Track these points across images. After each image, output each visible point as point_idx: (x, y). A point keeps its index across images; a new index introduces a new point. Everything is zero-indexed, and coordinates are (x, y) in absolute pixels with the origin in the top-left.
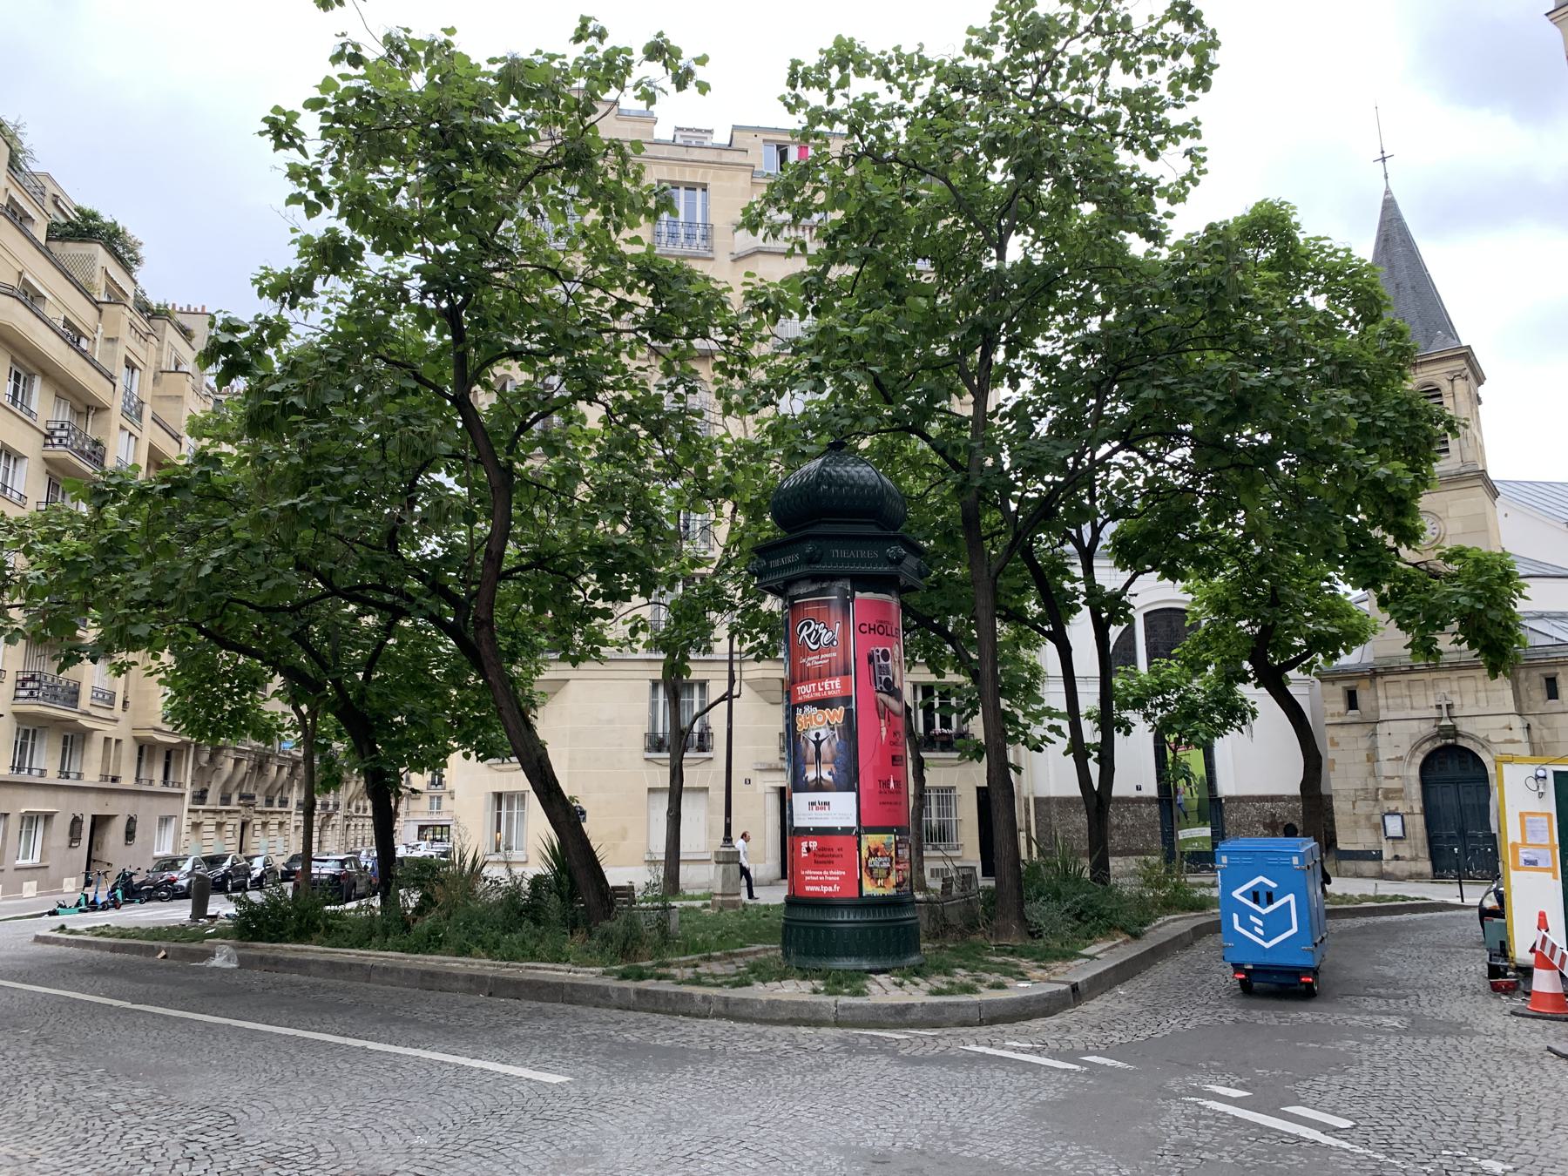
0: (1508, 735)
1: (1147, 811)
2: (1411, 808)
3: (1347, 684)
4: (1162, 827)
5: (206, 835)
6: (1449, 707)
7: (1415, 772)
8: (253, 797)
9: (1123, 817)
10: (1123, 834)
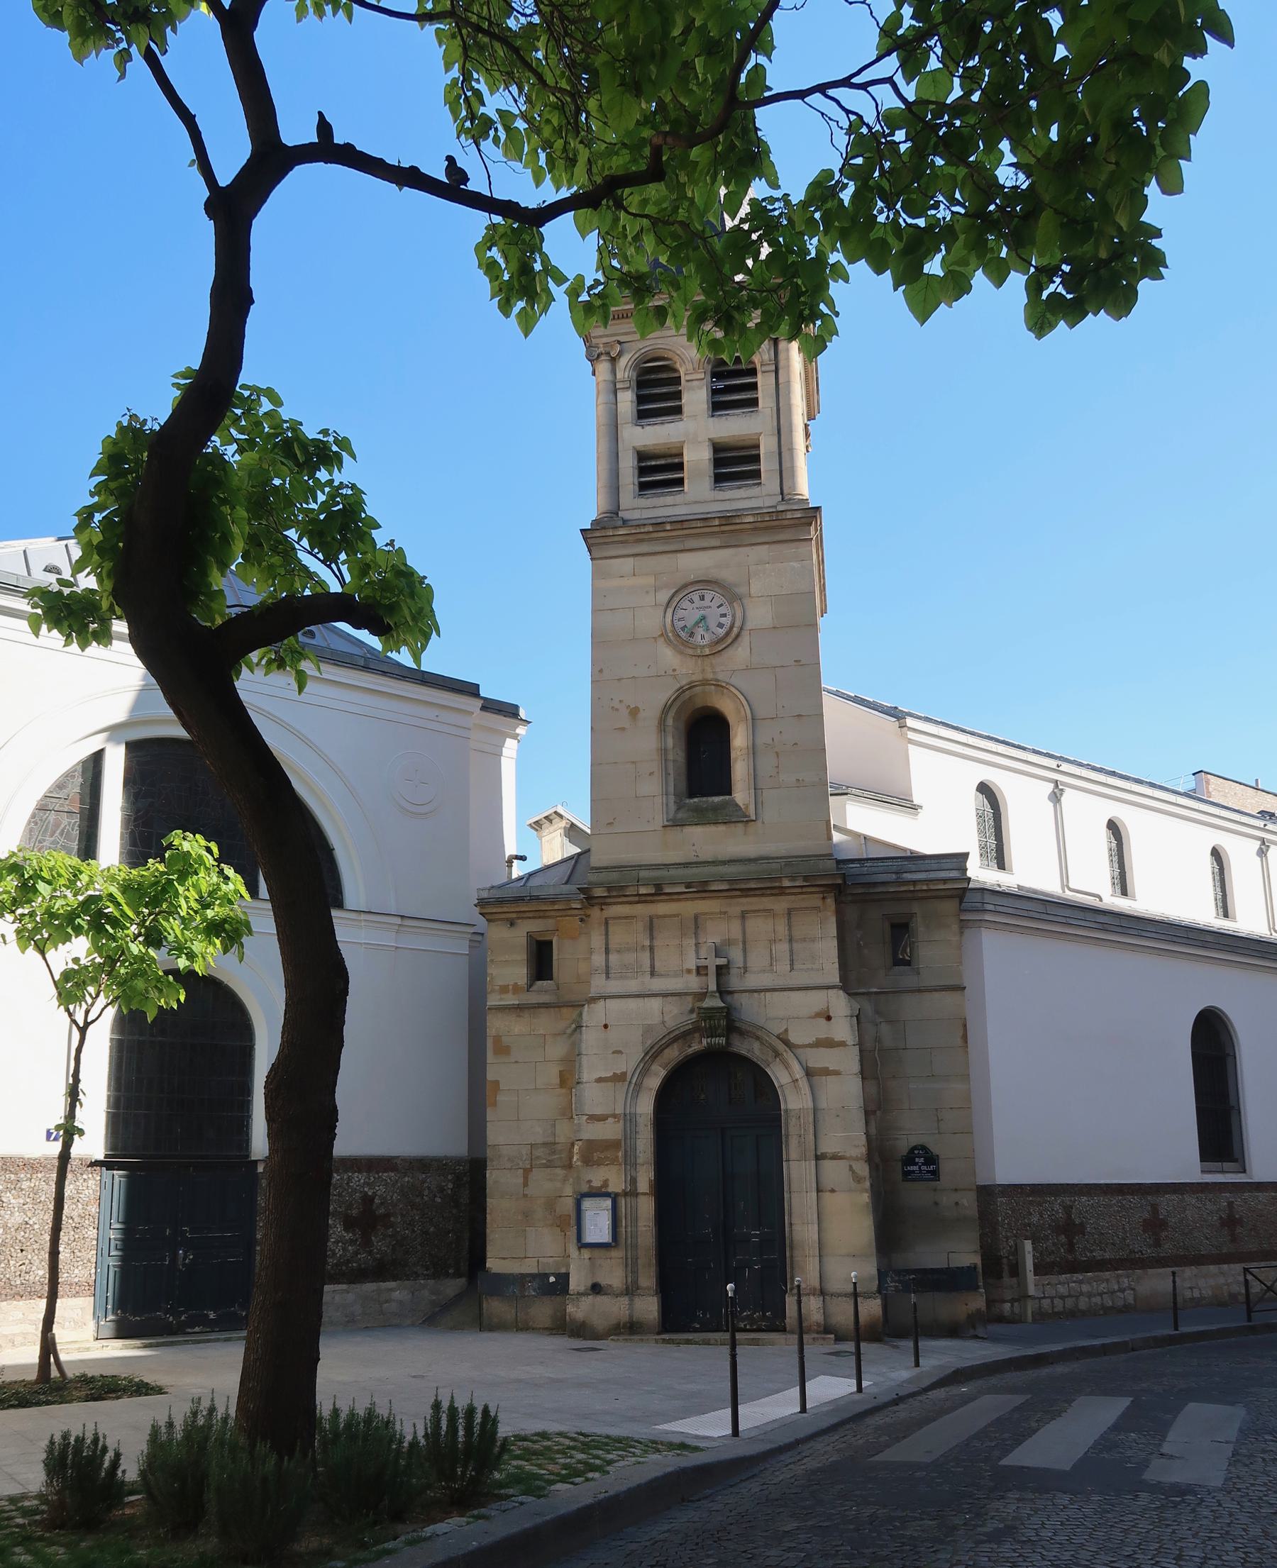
0: (821, 1030)
3: (530, 926)
6: (722, 971)
7: (646, 1106)
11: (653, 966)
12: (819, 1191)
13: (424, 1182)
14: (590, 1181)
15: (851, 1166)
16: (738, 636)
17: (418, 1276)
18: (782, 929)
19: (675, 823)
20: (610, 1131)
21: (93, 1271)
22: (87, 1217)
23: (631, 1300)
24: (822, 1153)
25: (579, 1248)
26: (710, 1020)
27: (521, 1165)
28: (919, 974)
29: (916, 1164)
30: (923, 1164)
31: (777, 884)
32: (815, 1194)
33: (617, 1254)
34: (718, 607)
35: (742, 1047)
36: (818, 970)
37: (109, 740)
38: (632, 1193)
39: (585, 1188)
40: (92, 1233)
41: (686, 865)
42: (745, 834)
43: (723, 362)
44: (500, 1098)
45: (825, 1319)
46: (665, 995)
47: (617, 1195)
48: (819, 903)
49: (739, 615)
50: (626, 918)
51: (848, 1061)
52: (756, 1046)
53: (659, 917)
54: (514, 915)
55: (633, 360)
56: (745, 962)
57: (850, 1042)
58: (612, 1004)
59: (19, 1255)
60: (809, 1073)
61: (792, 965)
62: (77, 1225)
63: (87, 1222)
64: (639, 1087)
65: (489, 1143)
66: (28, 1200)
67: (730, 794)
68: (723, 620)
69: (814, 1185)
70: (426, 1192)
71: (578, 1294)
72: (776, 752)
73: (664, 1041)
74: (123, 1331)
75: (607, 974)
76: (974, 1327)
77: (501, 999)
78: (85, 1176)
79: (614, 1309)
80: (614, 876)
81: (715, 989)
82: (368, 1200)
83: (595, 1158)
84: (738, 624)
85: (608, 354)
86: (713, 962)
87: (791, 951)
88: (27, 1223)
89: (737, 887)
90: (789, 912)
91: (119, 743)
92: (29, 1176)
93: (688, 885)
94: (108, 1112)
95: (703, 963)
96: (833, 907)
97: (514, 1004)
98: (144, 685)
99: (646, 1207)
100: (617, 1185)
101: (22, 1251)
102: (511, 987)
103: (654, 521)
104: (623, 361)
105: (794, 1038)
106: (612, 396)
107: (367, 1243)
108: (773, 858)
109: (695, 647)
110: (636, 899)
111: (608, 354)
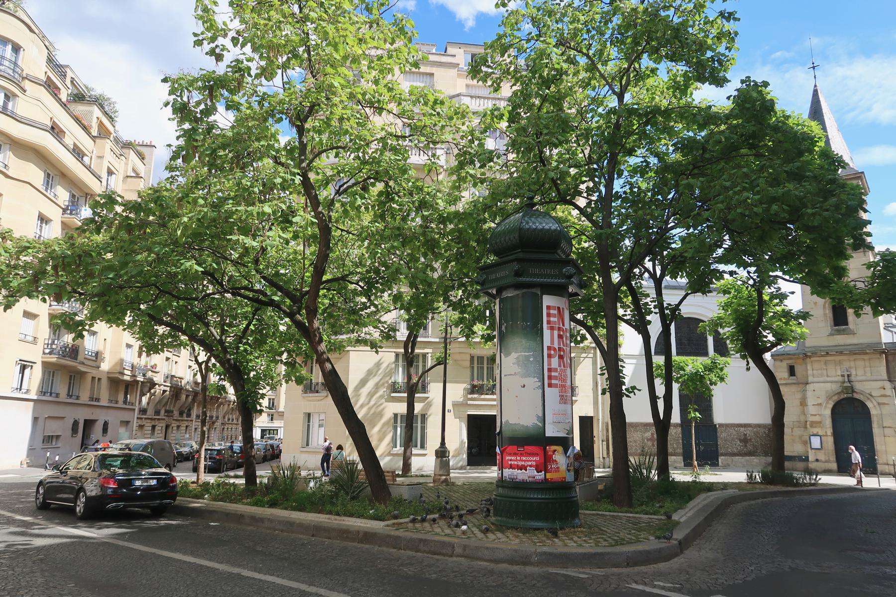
0: (882, 392)
1: (674, 431)
2: (826, 432)
4: (683, 440)
5: (146, 432)
8: (173, 412)
19: (831, 335)
33: (823, 451)
41: (836, 346)
52: (862, 396)
60: (879, 404)
80: (813, 349)
86: (846, 373)
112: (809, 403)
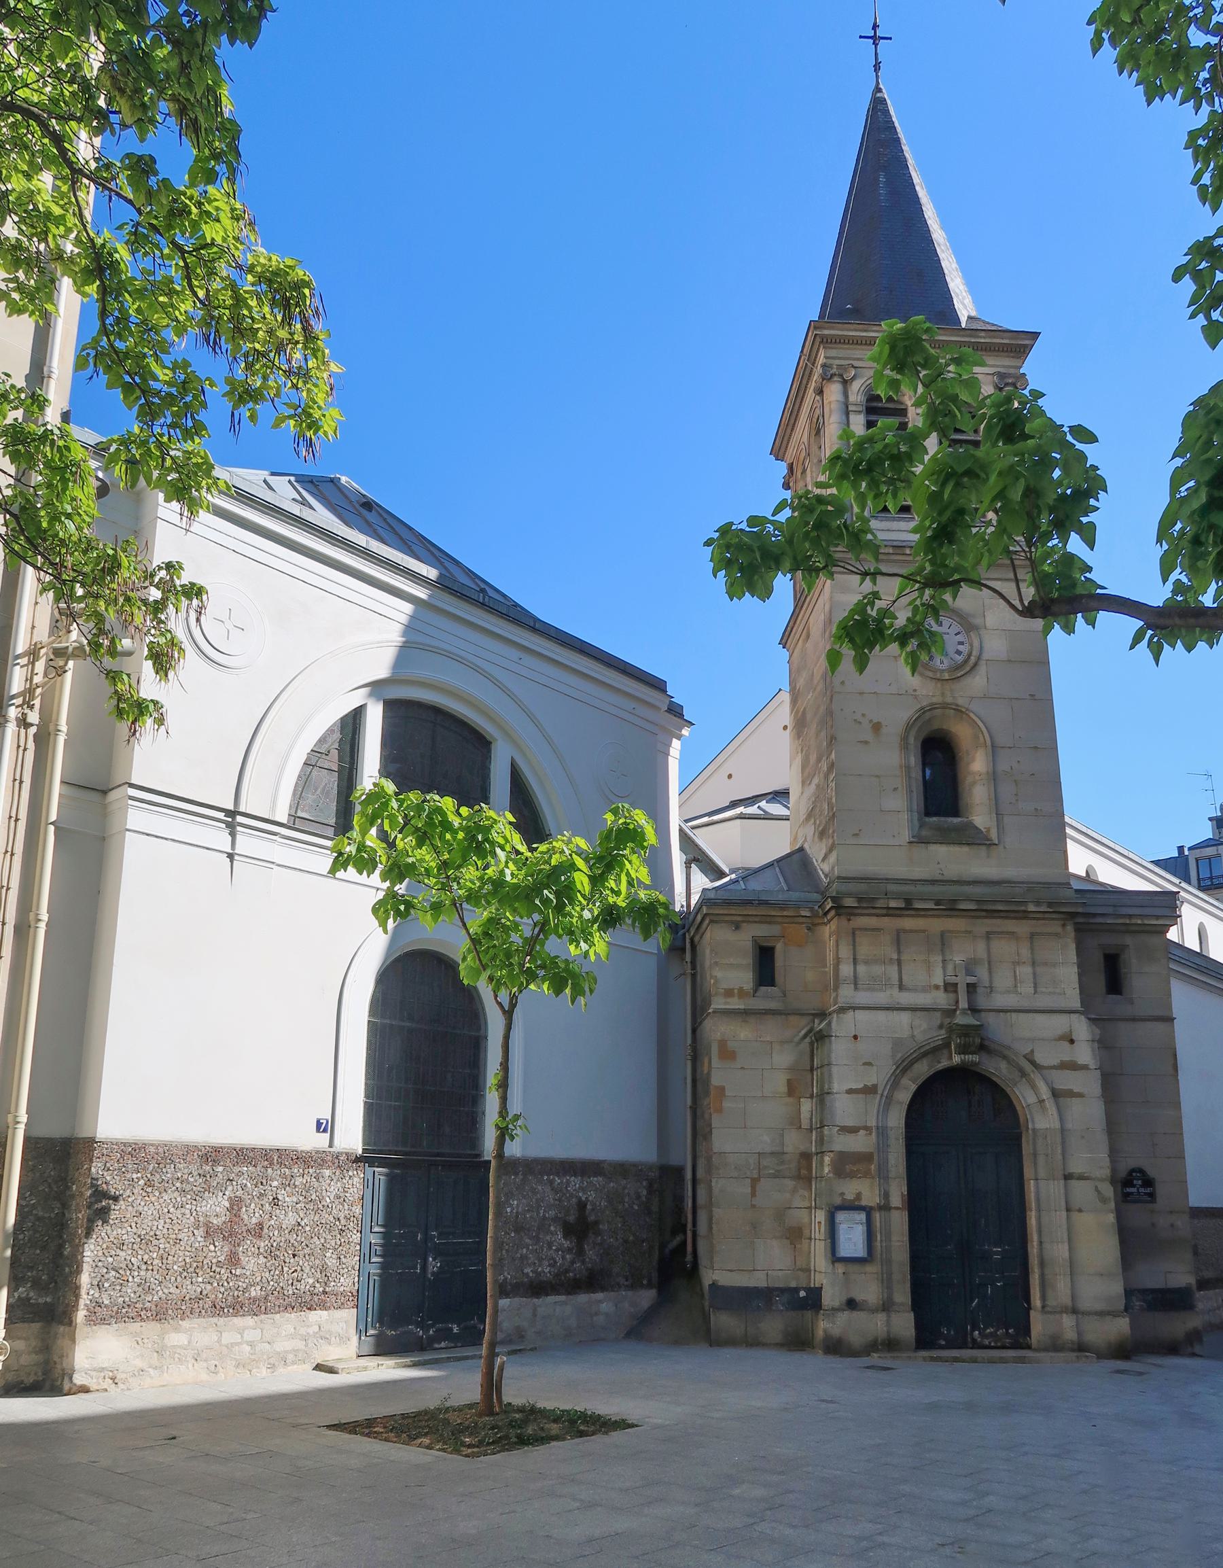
0: (1064, 1053)
1: (335, 1188)
3: (761, 931)
6: (971, 988)
7: (896, 1120)
9: (275, 1202)
10: (271, 1254)
11: (901, 980)
12: (1068, 1210)
13: (624, 1188)
14: (843, 1194)
15: (1096, 1187)
16: (976, 665)
17: (620, 1287)
18: (1025, 952)
19: (920, 840)
20: (859, 1143)
21: (356, 1279)
22: (352, 1218)
23: (889, 1316)
24: (1069, 1173)
25: (833, 1262)
26: (965, 1037)
27: (748, 1174)
28: (1132, 1003)
29: (1134, 1186)
30: (1142, 1186)
31: (1023, 908)
32: (1064, 1214)
33: (870, 1268)
34: (956, 634)
35: (996, 1069)
36: (1060, 994)
37: (371, 695)
38: (885, 1207)
39: (838, 1201)
40: (356, 1237)
41: (933, 882)
42: (988, 857)
43: (878, 398)
44: (727, 1104)
45: (1078, 1338)
46: (913, 1009)
47: (871, 1208)
48: (1059, 930)
49: (976, 644)
50: (873, 930)
51: (1089, 1084)
52: (1003, 1065)
53: (905, 931)
54: (739, 919)
55: (865, 385)
56: (991, 981)
57: (1092, 1066)
58: (860, 1015)
59: (292, 1260)
60: (1056, 1094)
61: (1035, 987)
62: (343, 1228)
63: (351, 1223)
64: (889, 1101)
65: (715, 1150)
66: (301, 1198)
67: (956, 813)
68: (961, 648)
69: (1063, 1204)
70: (626, 1200)
71: (833, 1309)
72: (1015, 781)
73: (914, 1056)
74: (383, 1348)
75: (856, 984)
76: (1192, 1345)
77: (726, 1003)
78: (350, 1173)
79: (875, 1325)
80: (862, 887)
81: (967, 1006)
82: (582, 1206)
83: (848, 1171)
84: (975, 653)
85: (841, 376)
86: (962, 980)
87: (1034, 974)
88: (299, 1224)
89: (985, 908)
90: (1032, 936)
91: (378, 699)
92: (301, 1171)
93: (938, 902)
94: (365, 1103)
95: (953, 980)
96: (1073, 934)
97: (739, 1009)
98: (405, 642)
99: (899, 1222)
100: (871, 1197)
101: (294, 1256)
102: (736, 991)
103: (895, 544)
104: (856, 386)
105: (1040, 1058)
106: (844, 417)
107: (580, 1252)
108: (1014, 883)
109: (935, 671)
110: (884, 912)
111: (841, 376)
112: (836, 1087)
